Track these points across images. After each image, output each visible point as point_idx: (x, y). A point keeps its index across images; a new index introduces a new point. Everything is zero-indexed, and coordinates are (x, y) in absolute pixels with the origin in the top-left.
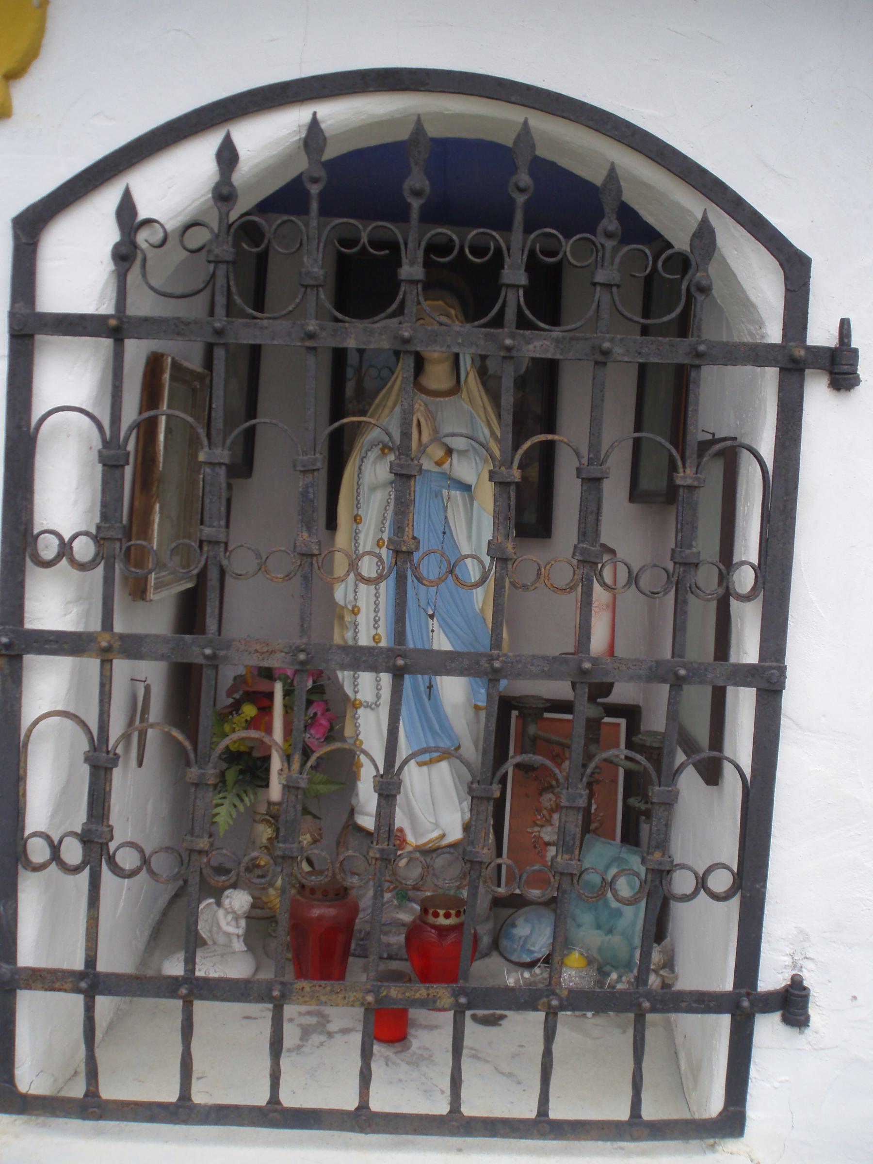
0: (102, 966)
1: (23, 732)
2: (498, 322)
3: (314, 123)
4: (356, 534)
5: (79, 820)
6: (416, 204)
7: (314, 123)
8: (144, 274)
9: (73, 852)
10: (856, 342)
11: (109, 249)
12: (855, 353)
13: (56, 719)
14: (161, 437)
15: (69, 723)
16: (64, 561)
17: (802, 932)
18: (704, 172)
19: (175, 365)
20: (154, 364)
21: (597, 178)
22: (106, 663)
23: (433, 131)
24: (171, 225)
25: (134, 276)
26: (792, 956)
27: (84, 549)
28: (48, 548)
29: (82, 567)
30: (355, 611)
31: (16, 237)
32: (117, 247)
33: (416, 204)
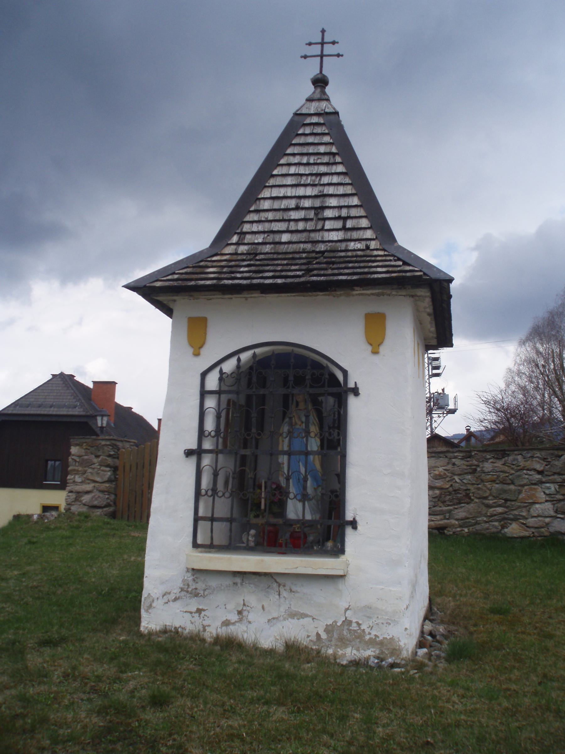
0: (215, 516)
1: (202, 468)
2: (288, 388)
3: (254, 352)
4: (283, 446)
5: (211, 486)
6: (273, 366)
7: (254, 352)
8: (224, 383)
9: (210, 493)
10: (358, 386)
11: (218, 378)
12: (358, 388)
13: (208, 466)
14: (230, 416)
15: (210, 467)
16: (209, 436)
17: (355, 508)
18: (321, 353)
19: (233, 401)
20: (229, 401)
21: (325, 365)
22: (217, 455)
23: (276, 352)
24: (229, 373)
25: (222, 383)
26: (354, 514)
27: (213, 434)
28: (206, 433)
29: (213, 437)
30: (283, 464)
31: (201, 377)
32: (219, 378)
33: (273, 366)
